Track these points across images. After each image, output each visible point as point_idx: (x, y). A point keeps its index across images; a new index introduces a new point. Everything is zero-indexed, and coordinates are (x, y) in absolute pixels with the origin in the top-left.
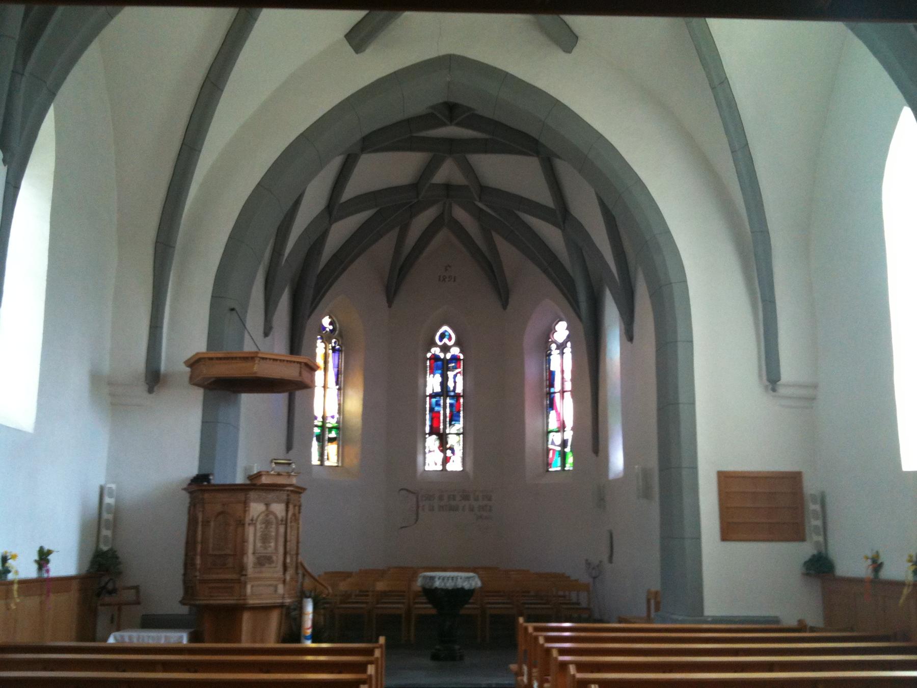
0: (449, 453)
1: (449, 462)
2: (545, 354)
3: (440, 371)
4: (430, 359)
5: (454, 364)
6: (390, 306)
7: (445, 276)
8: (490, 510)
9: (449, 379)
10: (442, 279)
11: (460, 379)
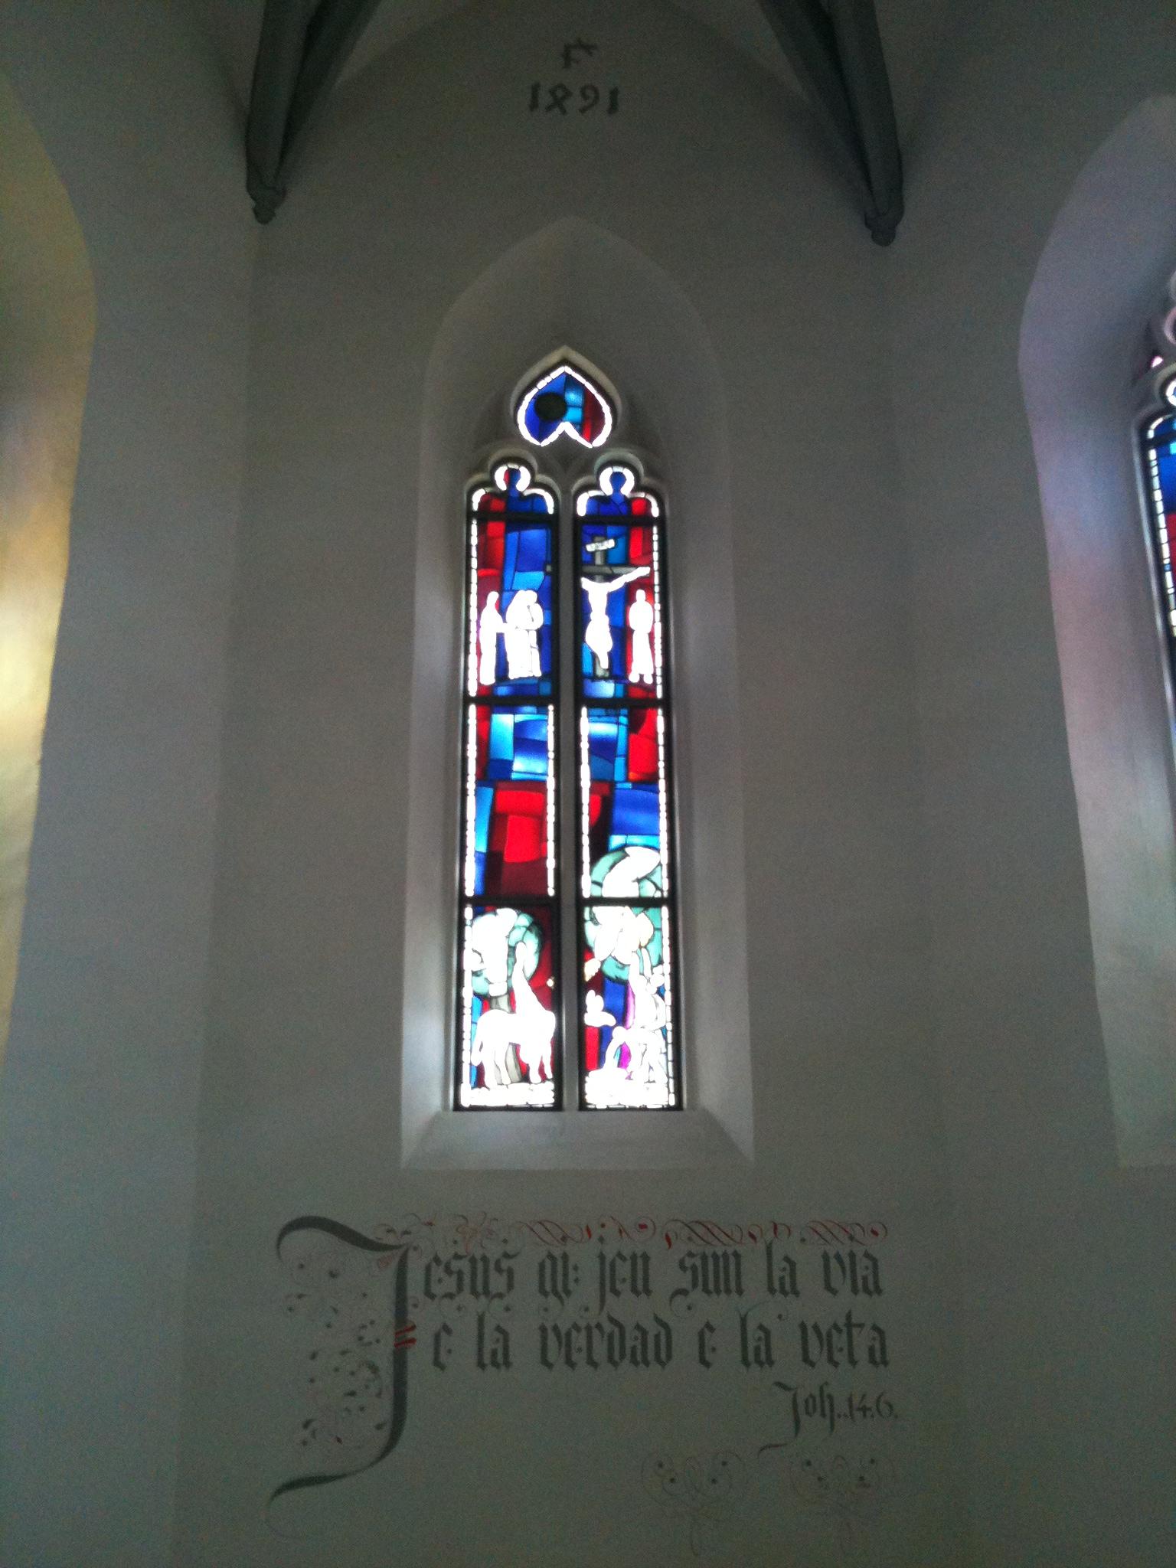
0: (595, 1012)
1: (599, 1061)
2: (1135, 440)
3: (538, 577)
4: (484, 515)
5: (610, 544)
6: (264, 213)
7: (561, 86)
8: (879, 1358)
9: (592, 616)
10: (545, 99)
11: (643, 615)
